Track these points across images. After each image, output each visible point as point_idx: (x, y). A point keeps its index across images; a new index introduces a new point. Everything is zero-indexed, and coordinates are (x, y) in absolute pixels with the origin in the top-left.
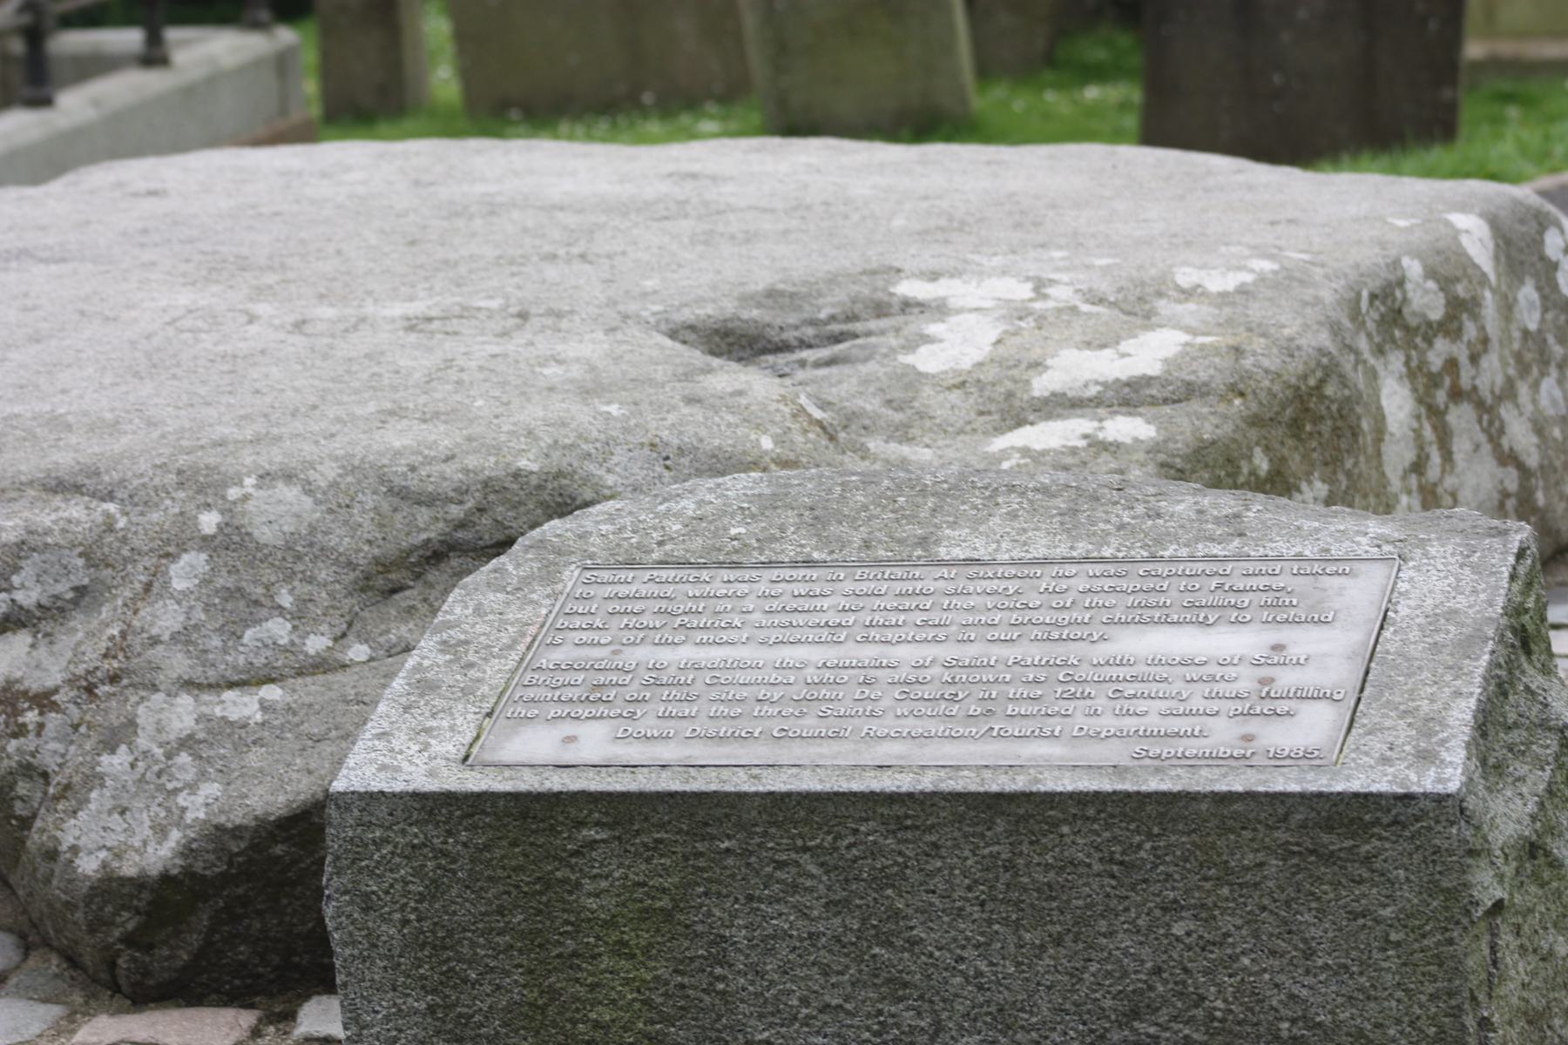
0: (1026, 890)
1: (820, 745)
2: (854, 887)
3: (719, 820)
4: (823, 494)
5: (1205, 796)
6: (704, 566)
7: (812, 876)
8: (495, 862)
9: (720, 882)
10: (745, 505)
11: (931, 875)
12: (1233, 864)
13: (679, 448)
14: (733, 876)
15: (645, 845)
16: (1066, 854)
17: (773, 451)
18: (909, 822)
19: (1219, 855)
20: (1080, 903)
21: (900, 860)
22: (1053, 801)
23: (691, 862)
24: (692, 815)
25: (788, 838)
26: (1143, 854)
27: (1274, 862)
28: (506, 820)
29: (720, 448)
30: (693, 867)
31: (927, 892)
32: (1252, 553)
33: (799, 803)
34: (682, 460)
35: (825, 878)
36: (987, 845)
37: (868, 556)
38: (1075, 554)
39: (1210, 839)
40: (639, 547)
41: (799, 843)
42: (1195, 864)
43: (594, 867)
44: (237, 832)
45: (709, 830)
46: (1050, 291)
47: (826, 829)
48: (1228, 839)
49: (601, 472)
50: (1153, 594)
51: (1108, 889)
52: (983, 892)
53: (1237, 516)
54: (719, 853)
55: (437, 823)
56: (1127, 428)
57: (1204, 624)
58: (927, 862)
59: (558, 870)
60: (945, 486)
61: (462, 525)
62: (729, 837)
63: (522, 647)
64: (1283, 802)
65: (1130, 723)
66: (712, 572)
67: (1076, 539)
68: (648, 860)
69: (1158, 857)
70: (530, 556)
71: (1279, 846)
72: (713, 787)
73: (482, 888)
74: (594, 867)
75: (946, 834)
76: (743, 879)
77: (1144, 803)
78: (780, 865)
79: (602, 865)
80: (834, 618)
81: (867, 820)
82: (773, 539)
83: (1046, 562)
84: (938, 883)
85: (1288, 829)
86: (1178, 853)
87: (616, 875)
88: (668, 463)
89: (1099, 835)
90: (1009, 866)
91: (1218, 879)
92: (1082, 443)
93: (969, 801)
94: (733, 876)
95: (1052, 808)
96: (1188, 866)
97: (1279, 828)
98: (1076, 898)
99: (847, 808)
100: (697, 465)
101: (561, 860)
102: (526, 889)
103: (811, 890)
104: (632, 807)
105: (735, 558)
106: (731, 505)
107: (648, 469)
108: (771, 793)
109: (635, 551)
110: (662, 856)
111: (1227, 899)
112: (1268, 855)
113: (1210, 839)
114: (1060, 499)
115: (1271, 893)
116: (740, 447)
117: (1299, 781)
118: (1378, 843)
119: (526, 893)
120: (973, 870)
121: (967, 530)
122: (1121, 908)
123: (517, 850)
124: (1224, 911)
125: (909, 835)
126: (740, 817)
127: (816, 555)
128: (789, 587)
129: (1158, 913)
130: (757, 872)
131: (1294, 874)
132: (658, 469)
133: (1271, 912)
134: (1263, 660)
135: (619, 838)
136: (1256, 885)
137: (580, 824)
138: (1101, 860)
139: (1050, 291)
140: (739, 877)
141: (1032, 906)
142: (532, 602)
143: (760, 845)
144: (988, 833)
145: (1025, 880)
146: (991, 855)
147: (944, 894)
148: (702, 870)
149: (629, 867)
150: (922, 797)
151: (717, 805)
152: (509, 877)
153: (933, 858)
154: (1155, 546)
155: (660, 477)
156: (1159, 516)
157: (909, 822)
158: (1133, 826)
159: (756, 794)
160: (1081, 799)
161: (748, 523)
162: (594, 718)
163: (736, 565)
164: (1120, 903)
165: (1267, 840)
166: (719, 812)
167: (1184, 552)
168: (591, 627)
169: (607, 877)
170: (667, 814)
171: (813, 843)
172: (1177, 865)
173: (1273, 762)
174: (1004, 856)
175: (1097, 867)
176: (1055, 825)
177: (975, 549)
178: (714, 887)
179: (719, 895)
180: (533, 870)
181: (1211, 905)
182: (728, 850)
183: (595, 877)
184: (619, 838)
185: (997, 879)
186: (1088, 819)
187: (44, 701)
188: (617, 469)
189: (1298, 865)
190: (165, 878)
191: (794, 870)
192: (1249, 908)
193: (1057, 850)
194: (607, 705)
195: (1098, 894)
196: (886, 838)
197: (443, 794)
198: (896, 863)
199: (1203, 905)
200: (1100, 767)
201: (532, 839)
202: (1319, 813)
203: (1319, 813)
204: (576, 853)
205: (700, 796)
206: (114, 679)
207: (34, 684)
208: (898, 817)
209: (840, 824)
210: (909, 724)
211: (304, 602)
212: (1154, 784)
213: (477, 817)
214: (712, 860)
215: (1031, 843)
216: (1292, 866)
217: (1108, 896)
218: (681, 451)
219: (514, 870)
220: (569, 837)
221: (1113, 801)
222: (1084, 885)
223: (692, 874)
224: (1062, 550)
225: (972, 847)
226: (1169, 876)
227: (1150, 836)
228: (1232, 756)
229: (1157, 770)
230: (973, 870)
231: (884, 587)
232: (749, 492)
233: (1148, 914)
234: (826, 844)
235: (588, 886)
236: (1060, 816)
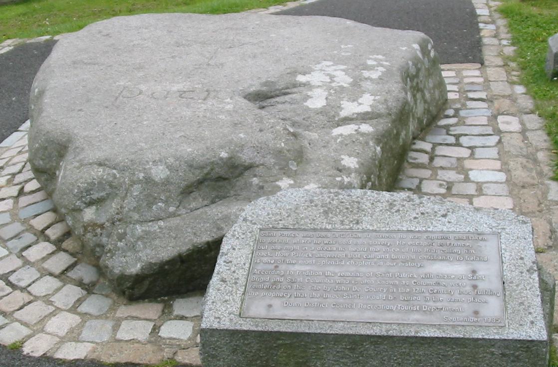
44: (155, 264)
46: (335, 79)
49: (241, 155)
56: (366, 128)
61: (207, 174)
64: (493, 341)
92: (354, 133)
118: (521, 352)
139: (335, 79)
175: (435, 356)
187: (102, 226)
188: (245, 154)
190: (137, 275)
206: (119, 221)
207: (99, 222)
211: (168, 198)
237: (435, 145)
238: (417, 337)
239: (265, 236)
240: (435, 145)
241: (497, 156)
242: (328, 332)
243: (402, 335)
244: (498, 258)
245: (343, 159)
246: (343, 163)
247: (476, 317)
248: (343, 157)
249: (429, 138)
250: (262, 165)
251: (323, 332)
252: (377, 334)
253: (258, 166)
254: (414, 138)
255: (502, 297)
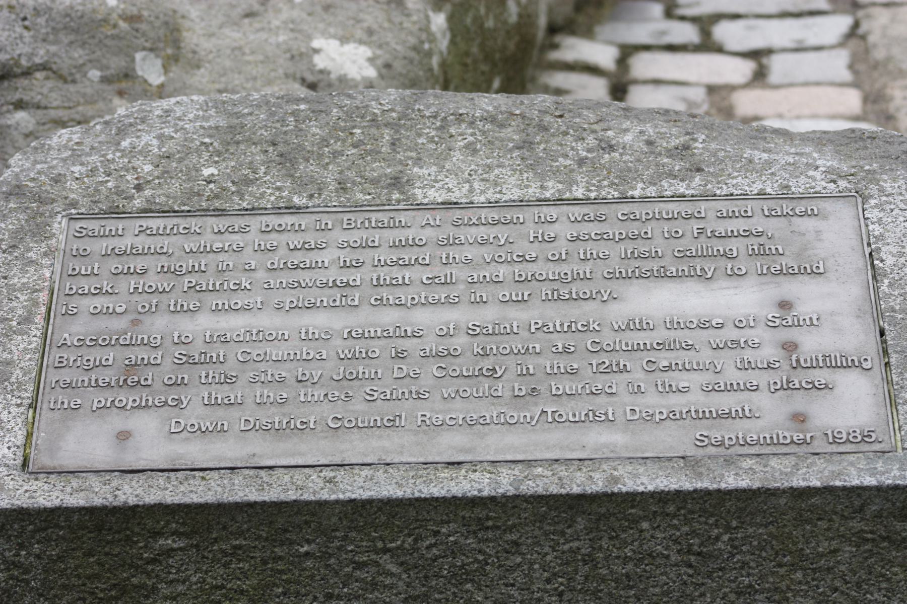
0: (603, 580)
1: (380, 437)
2: (434, 583)
3: (299, 526)
4: (278, 125)
5: (784, 491)
6: (188, 214)
7: (392, 575)
8: (69, 571)
9: (298, 583)
10: (207, 140)
11: (511, 569)
12: (808, 551)
13: (35, 9)
14: (312, 577)
15: (223, 551)
16: (645, 547)
17: (117, 7)
18: (490, 523)
19: (795, 544)
20: (657, 590)
21: (481, 558)
22: (634, 500)
23: (270, 566)
24: (271, 523)
25: (369, 540)
26: (720, 545)
27: (848, 548)
28: (80, 533)
29: (72, 8)
30: (272, 570)
31: (506, 585)
32: (718, 192)
33: (380, 509)
34: (39, 20)
35: (404, 576)
36: (567, 541)
37: (348, 200)
38: (548, 195)
39: (787, 530)
40: (119, 192)
41: (380, 545)
42: (771, 552)
43: (170, 573)
45: (288, 535)
47: (406, 532)
48: (804, 530)
50: (640, 241)
51: (685, 577)
52: (561, 584)
53: (686, 147)
54: (300, 556)
55: (9, 537)
57: (703, 277)
58: (507, 559)
59: (133, 576)
60: (394, 115)
62: (309, 542)
63: (39, 319)
64: (859, 495)
65: (676, 401)
66: (200, 221)
67: (542, 177)
68: (225, 566)
69: (736, 548)
70: (12, 205)
71: (853, 534)
72: (292, 496)
73: (55, 596)
74: (170, 573)
75: (527, 532)
76: (322, 579)
77: (724, 500)
78: (360, 566)
79: (179, 571)
80: (333, 274)
81: (448, 522)
82: (248, 182)
83: (521, 204)
84: (518, 577)
85: (862, 519)
86: (755, 543)
87: (194, 579)
88: (27, 23)
89: (679, 530)
90: (589, 560)
91: (793, 565)
93: (551, 503)
94: (312, 577)
95: (632, 507)
96: (764, 554)
97: (854, 518)
98: (653, 586)
99: (428, 513)
100: (52, 24)
101: (137, 567)
102: (102, 595)
103: (391, 587)
104: (210, 518)
105: (217, 204)
106: (193, 140)
107: (9, 30)
108: (352, 501)
109: (115, 197)
110: (240, 561)
111: (800, 583)
112: (841, 542)
113: (787, 530)
114: (510, 129)
115: (843, 577)
116: (89, 6)
117: (873, 472)
119: (101, 599)
120: (552, 564)
121: (434, 168)
122: (697, 594)
123: (92, 560)
124: (796, 593)
125: (490, 534)
126: (320, 524)
127: (296, 200)
128: (284, 237)
129: (732, 597)
130: (337, 573)
131: (866, 558)
132: (19, 30)
133: (842, 592)
134: (778, 321)
135: (197, 546)
136: (829, 569)
137: (157, 534)
138: (679, 552)
140: (318, 578)
141: (610, 594)
142: (31, 262)
143: (339, 548)
144: (569, 531)
145: (604, 571)
146: (571, 550)
147: (523, 587)
148: (281, 572)
149: (206, 572)
150: (504, 500)
151: (297, 513)
152: (84, 585)
153: (513, 554)
154: (622, 184)
155: (21, 37)
156: (611, 148)
157: (490, 523)
158: (711, 521)
159: (337, 502)
160: (662, 497)
161: (216, 162)
162: (139, 407)
163: (221, 213)
164: (696, 590)
165: (842, 529)
166: (298, 519)
167: (652, 191)
168: (100, 292)
169: (184, 582)
170: (246, 523)
171: (393, 545)
172: (753, 554)
173: (835, 448)
174: (583, 551)
175: (674, 558)
176: (636, 521)
177: (449, 190)
178: (293, 587)
179: (298, 594)
180: (109, 578)
181: (784, 588)
182: (307, 554)
183: (172, 582)
184: (197, 546)
185: (576, 571)
186: (667, 515)
189: (871, 550)
191: (373, 570)
192: (821, 590)
193: (635, 543)
194: (147, 390)
195: (674, 582)
196: (466, 538)
197: (15, 510)
198: (476, 561)
199: (777, 588)
200: (670, 459)
201: (107, 549)
202: (894, 504)
203: (894, 504)
204: (153, 561)
205: (279, 506)
208: (480, 519)
209: (421, 526)
210: (459, 410)
212: (731, 481)
213: (50, 530)
214: (292, 563)
215: (611, 538)
216: (865, 552)
217: (685, 583)
218: (37, 12)
219: (89, 578)
220: (146, 546)
221: (694, 499)
222: (662, 574)
223: (271, 576)
224: (533, 191)
225: (552, 543)
226: (745, 564)
227: (728, 528)
228: (792, 442)
229: (729, 462)
230: (552, 564)
231: (377, 235)
232: (206, 125)
233: (723, 598)
234: (406, 546)
235: (163, 588)
236: (641, 513)
237: (627, 52)
238: (613, 494)
239: (87, 235)
240: (627, 52)
241: (846, 76)
242: (325, 495)
243: (563, 491)
244: (861, 263)
245: (317, 51)
246: (320, 62)
247: (801, 432)
248: (316, 44)
249: (606, 30)
250: (44, 67)
251: (307, 496)
252: (485, 493)
253: (27, 73)
254: (553, 30)
255: (878, 370)
